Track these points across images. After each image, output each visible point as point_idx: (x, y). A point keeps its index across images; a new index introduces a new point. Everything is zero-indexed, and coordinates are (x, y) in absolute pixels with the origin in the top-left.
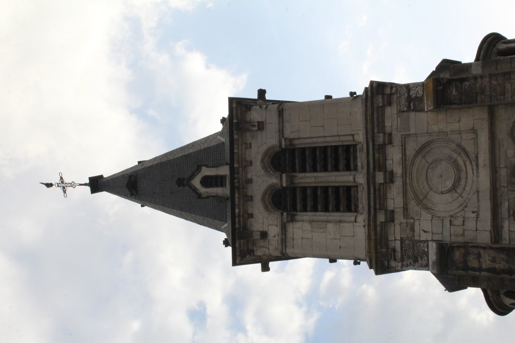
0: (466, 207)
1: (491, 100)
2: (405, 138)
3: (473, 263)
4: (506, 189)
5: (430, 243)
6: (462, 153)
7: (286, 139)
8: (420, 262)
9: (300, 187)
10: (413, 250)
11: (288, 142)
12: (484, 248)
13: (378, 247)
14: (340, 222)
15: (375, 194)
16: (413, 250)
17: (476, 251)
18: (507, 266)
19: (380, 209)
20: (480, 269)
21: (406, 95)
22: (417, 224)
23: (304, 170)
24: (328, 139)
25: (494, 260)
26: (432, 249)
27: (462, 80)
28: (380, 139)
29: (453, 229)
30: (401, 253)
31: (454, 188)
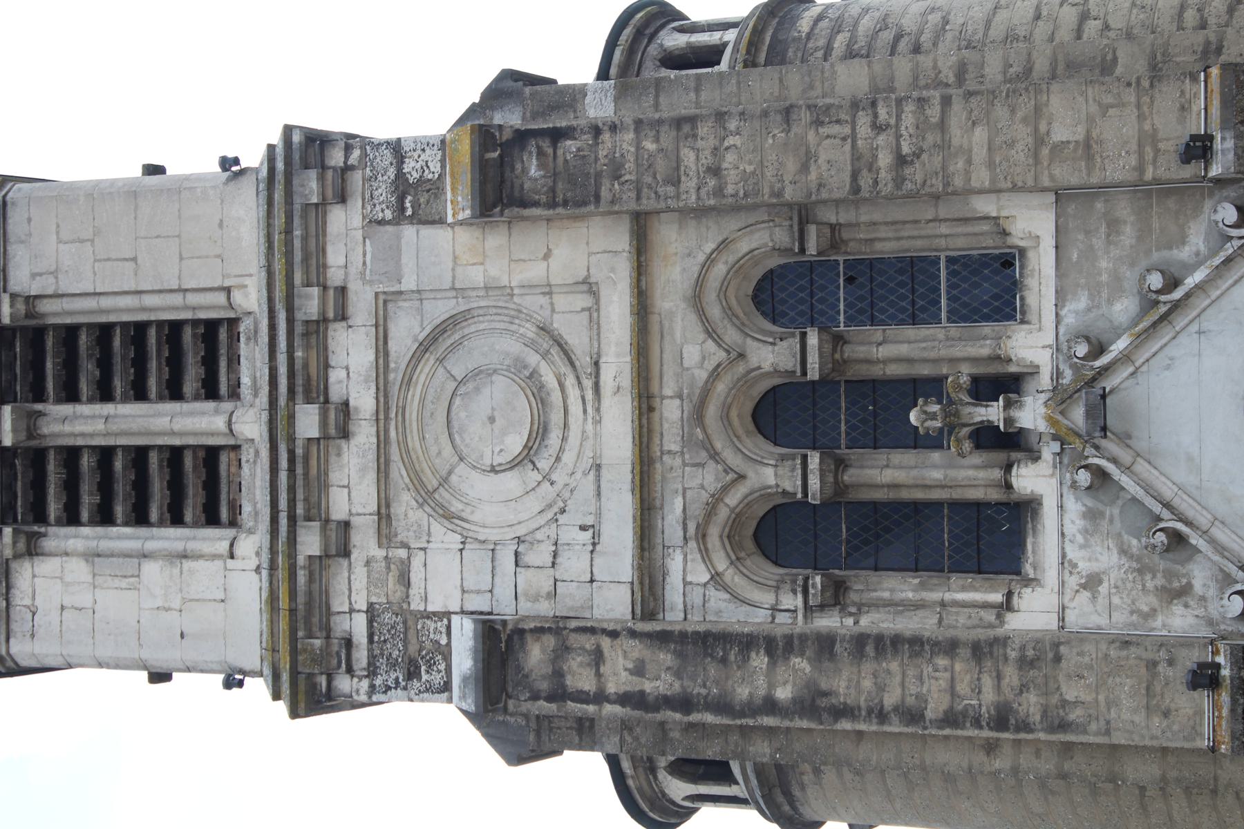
0: (563, 511)
1: (638, 198)
2: (385, 303)
3: (581, 678)
4: (678, 461)
5: (455, 620)
6: (555, 351)
7: (13, 296)
8: (425, 677)
9: (60, 449)
10: (406, 642)
11: (21, 307)
12: (614, 634)
13: (300, 634)
14: (184, 556)
15: (291, 470)
16: (406, 642)
17: (588, 642)
18: (677, 686)
19: (308, 518)
20: (600, 697)
21: (392, 172)
22: (417, 563)
23: (71, 395)
24: (150, 301)
25: (639, 670)
26: (463, 661)
27: (557, 135)
28: (310, 304)
29: (523, 575)
30: (370, 650)
31: (527, 456)
